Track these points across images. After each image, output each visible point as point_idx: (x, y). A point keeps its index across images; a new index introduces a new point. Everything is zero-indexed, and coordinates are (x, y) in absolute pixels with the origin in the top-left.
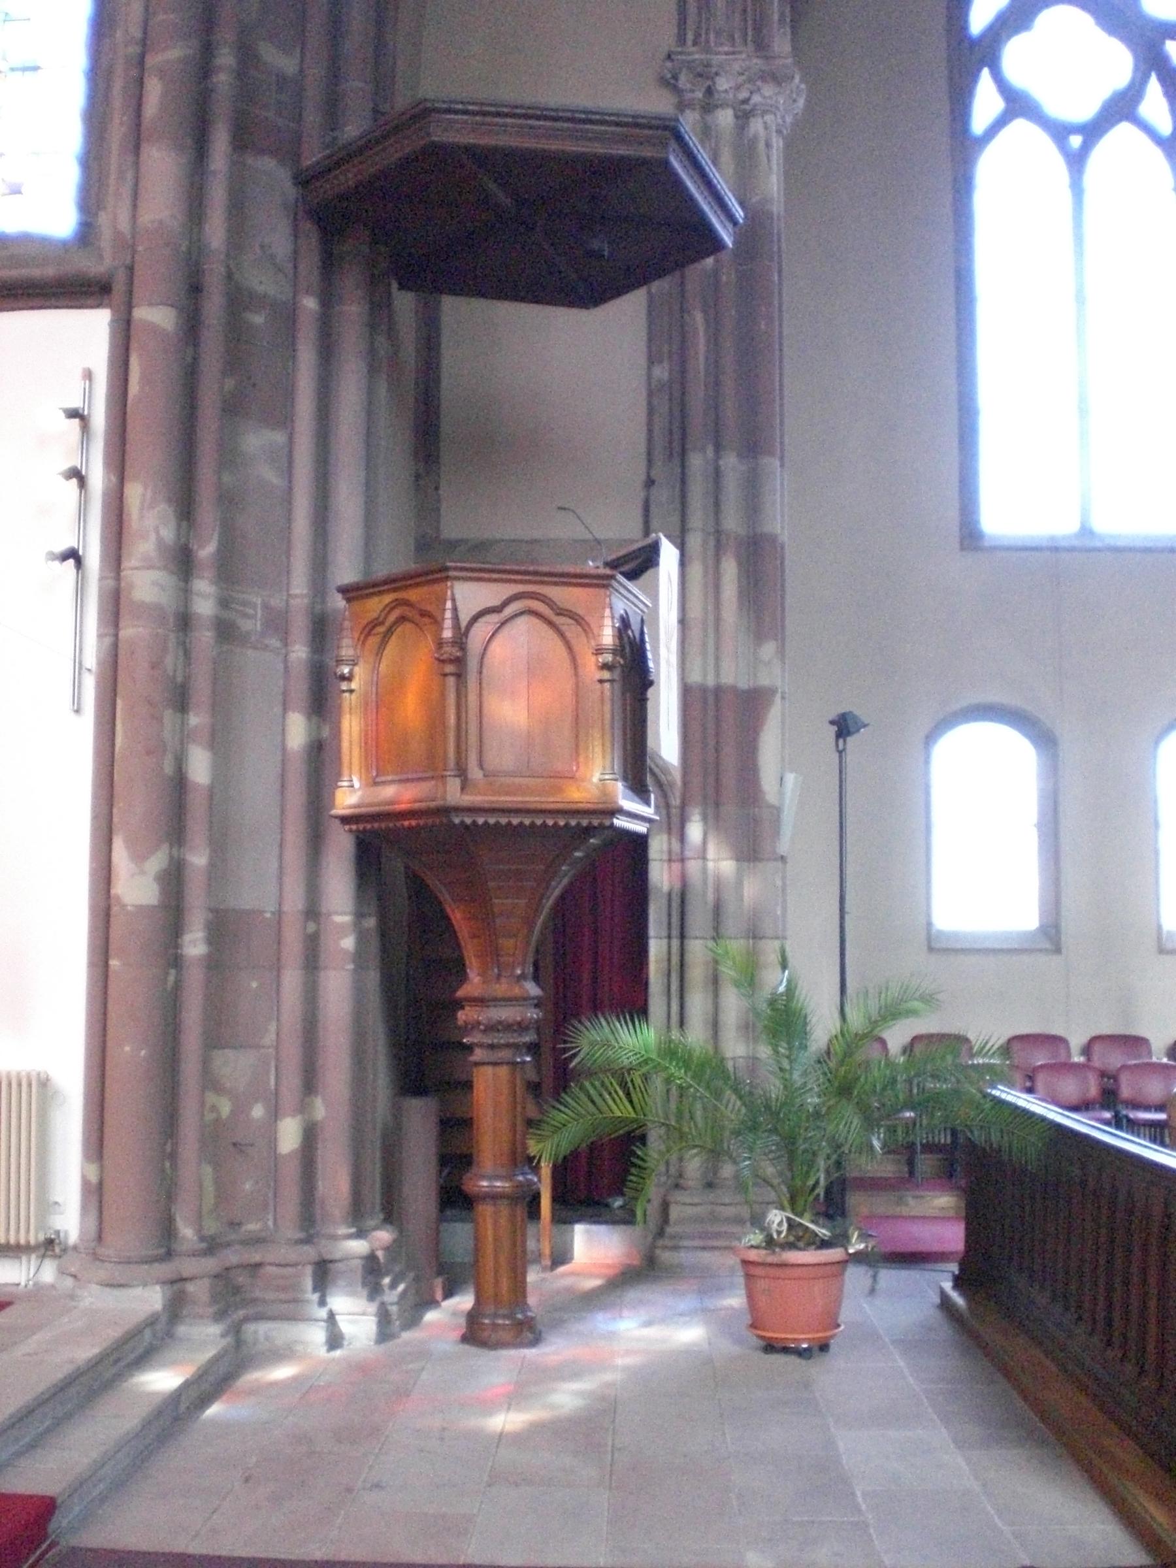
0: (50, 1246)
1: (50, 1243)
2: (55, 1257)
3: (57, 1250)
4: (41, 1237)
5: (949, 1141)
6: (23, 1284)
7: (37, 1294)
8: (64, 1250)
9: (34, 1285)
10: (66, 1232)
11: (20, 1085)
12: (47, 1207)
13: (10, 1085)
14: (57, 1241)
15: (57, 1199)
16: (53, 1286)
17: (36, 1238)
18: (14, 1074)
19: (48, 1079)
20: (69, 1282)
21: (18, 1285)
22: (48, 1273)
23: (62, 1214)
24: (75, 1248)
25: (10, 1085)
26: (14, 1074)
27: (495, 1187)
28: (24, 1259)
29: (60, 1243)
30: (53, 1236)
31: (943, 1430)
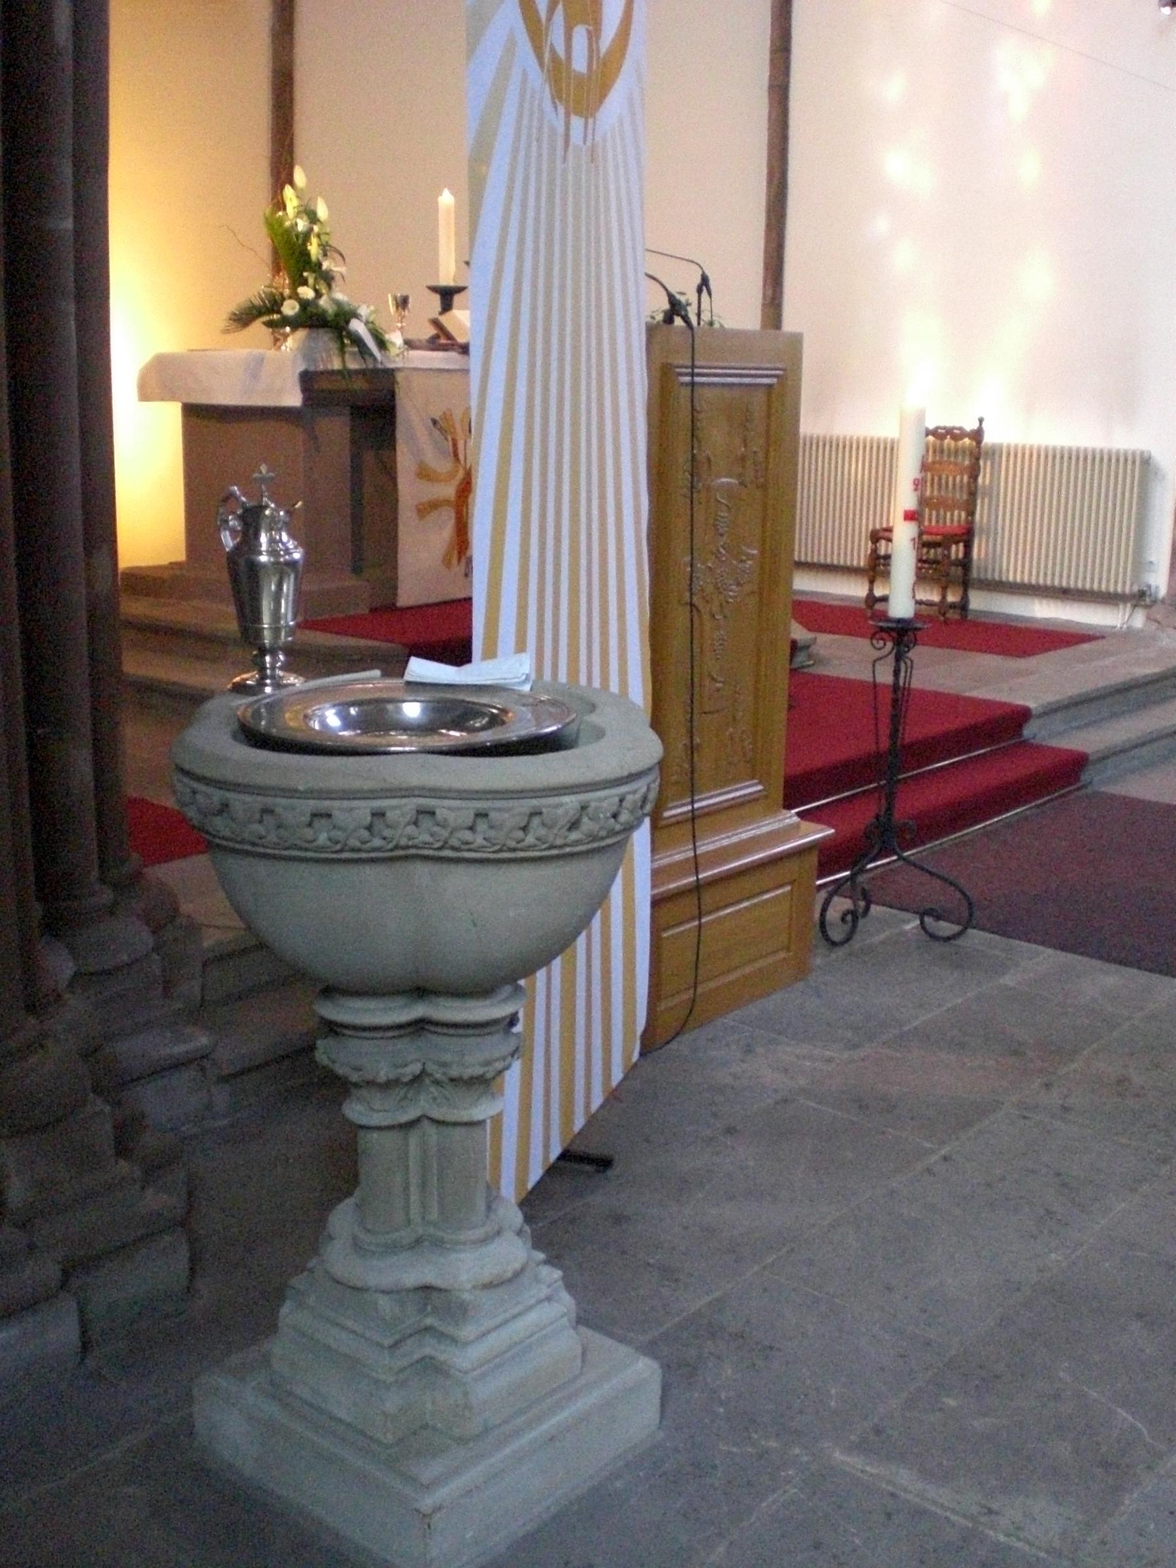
0: (1140, 598)
1: (1142, 594)
2: (1146, 607)
3: (1148, 600)
4: (1136, 588)
5: (961, 555)
6: (1119, 626)
7: (1126, 636)
8: (1155, 602)
9: (1128, 628)
10: (1157, 587)
11: (1062, 458)
12: (1140, 564)
13: (1009, 454)
14: (1148, 593)
15: (1153, 559)
16: (1142, 631)
17: (1131, 589)
18: (1106, 451)
19: (1150, 458)
20: (1154, 626)
21: (1115, 627)
22: (1139, 620)
23: (1153, 571)
24: (1163, 601)
25: (1009, 454)
26: (1106, 451)
27: (288, 593)
28: (1121, 607)
29: (1150, 595)
30: (1145, 589)
31: (462, 1256)
